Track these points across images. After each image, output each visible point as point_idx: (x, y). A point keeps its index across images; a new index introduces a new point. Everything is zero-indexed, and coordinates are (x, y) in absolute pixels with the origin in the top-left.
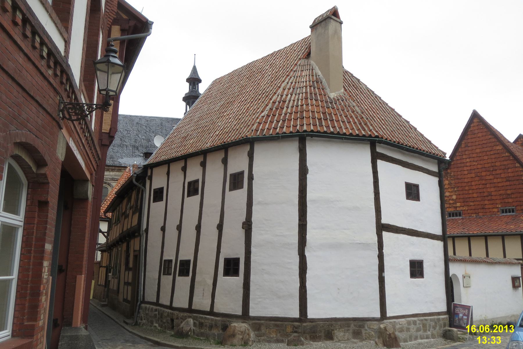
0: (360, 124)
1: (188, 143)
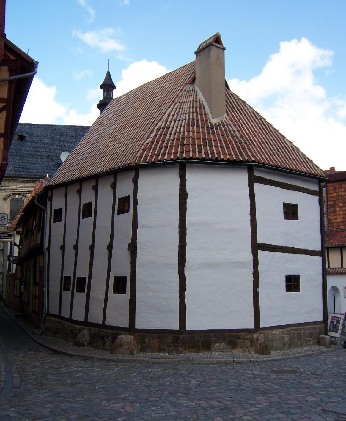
0: (239, 149)
1: (83, 166)
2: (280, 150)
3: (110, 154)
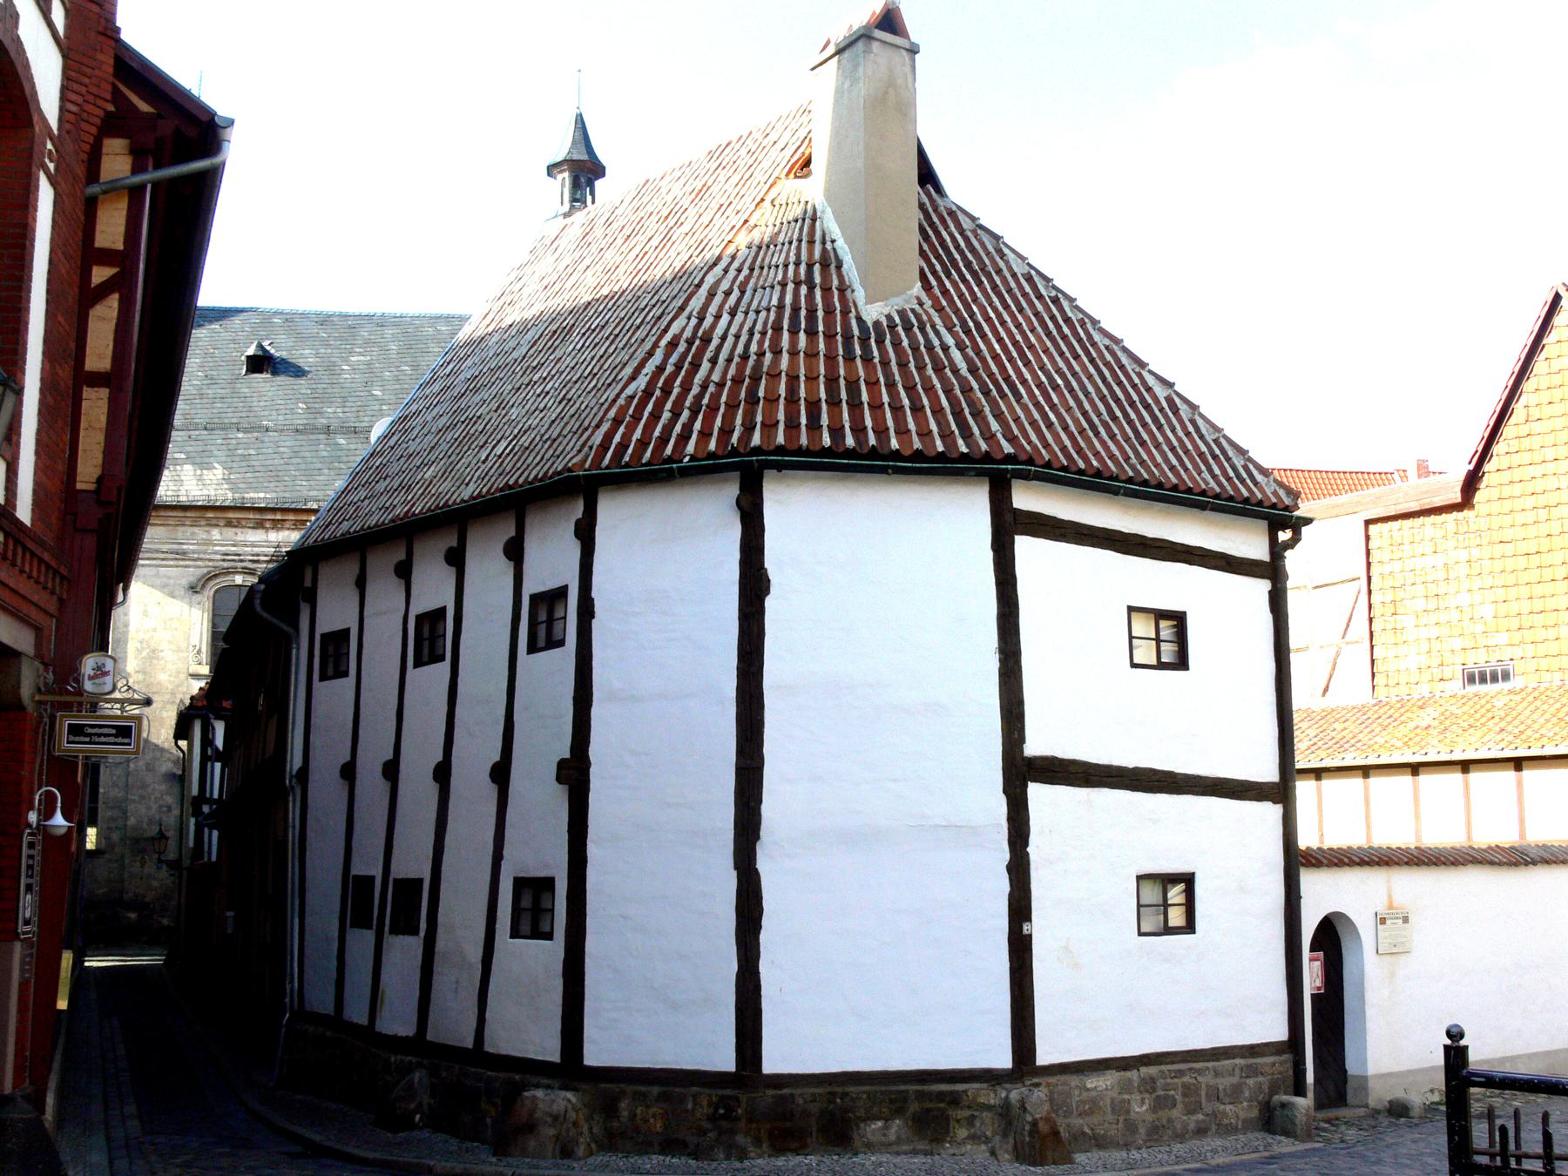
0: (958, 414)
2: (1118, 414)
3: (507, 434)
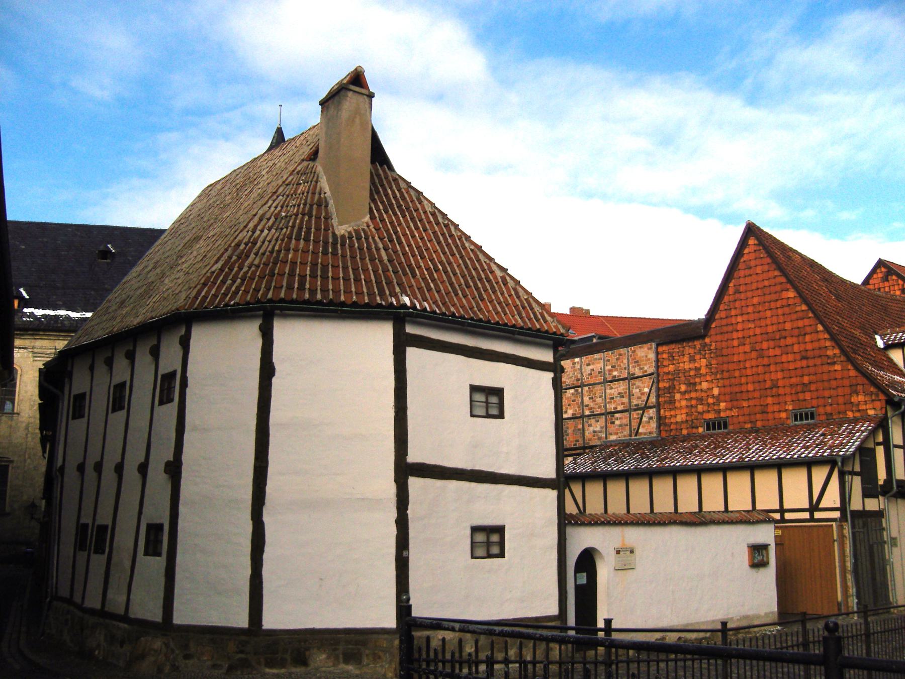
0: (379, 283)
